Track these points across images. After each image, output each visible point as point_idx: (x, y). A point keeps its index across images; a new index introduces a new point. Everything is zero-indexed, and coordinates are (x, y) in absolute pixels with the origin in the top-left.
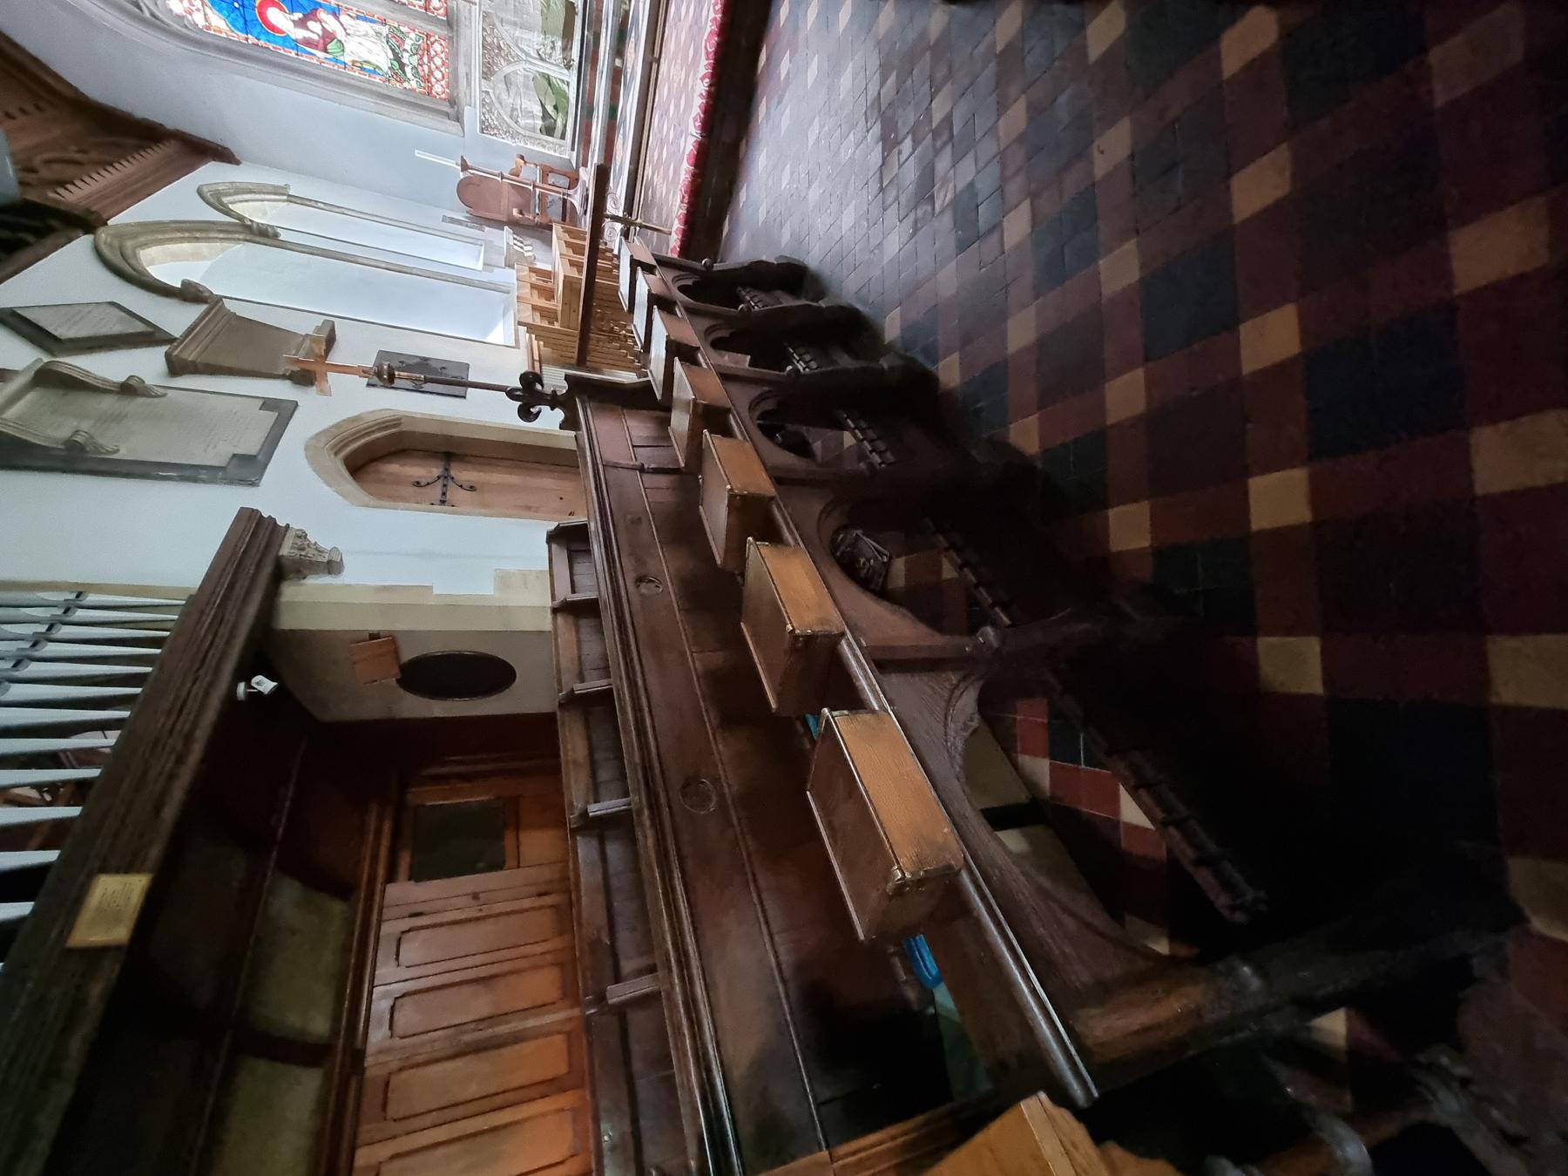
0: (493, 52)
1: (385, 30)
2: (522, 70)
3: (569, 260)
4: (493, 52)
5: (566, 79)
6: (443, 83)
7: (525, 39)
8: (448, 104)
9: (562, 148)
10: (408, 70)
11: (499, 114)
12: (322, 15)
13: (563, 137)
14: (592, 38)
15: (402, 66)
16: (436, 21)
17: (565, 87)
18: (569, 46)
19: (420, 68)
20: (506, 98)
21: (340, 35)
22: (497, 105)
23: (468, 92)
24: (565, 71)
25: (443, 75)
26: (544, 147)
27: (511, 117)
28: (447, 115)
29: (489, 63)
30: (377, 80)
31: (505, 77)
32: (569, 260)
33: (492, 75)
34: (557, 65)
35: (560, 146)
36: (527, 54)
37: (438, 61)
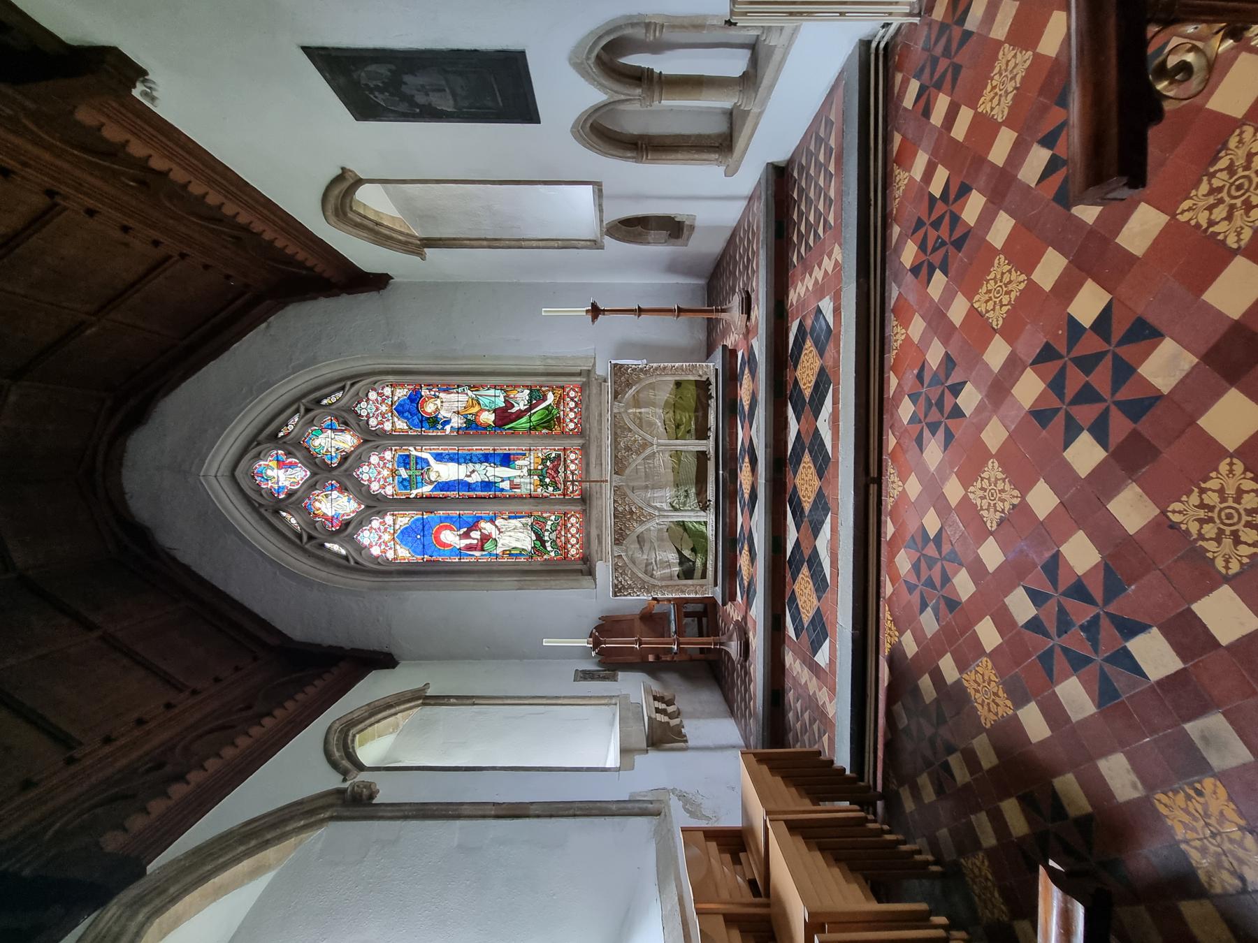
0: (624, 519)
1: (530, 521)
2: (656, 526)
3: (786, 821)
4: (624, 519)
6: (577, 546)
8: (581, 562)
10: (548, 544)
11: (633, 573)
12: (483, 524)
13: (704, 576)
15: (543, 543)
16: (573, 501)
18: (704, 489)
19: (558, 540)
21: (495, 533)
22: (631, 565)
24: (703, 513)
25: (577, 539)
26: (683, 592)
27: (646, 572)
28: (581, 572)
29: (621, 529)
30: (522, 560)
31: (638, 537)
32: (786, 821)
34: (692, 510)
35: (702, 586)
36: (660, 510)
37: (573, 530)
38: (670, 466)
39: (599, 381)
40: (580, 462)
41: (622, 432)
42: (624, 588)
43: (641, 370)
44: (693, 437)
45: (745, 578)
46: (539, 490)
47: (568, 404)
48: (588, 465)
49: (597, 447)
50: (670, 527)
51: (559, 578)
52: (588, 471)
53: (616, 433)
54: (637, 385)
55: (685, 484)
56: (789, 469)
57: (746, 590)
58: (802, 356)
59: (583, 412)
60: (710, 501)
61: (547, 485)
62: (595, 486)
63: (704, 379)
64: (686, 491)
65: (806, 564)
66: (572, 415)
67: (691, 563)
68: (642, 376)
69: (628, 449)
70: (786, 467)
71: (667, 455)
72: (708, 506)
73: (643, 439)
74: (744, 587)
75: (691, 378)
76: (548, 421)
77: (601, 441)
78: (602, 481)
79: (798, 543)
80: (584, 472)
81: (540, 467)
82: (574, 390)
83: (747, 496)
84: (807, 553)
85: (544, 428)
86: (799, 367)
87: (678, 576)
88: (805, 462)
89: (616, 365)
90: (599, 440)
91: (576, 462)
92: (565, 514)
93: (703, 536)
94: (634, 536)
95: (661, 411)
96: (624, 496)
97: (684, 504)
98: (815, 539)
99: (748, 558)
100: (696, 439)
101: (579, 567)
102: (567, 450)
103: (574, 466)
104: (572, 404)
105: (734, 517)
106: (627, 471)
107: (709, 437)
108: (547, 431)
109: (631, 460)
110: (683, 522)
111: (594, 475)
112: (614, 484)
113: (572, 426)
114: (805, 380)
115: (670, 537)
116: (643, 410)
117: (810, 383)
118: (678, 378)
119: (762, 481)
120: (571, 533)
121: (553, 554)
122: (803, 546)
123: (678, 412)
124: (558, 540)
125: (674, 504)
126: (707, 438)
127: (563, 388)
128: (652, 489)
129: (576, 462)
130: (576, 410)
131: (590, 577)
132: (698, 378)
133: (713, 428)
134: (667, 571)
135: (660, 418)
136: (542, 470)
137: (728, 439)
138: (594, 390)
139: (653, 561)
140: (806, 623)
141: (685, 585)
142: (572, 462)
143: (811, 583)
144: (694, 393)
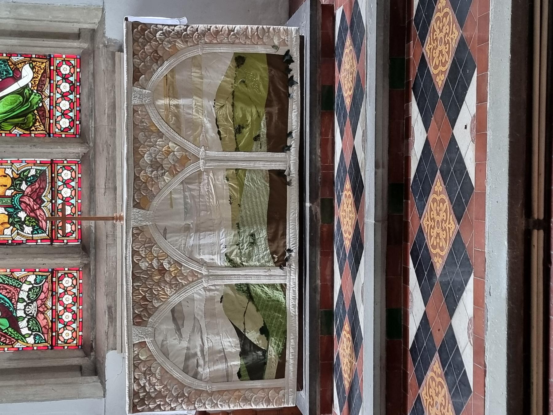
2: (202, 292)
5: (278, 281)
6: (74, 326)
7: (204, 245)
8: (80, 353)
9: (282, 392)
10: (23, 324)
11: (164, 371)
13: (280, 373)
14: (319, 210)
16: (67, 251)
17: (279, 295)
18: (280, 233)
19: (41, 316)
20: (176, 342)
22: (160, 359)
23: (111, 329)
24: (278, 271)
26: (246, 400)
27: (186, 370)
28: (80, 369)
29: (144, 298)
31: (173, 311)
33: (150, 315)
34: (262, 266)
35: (277, 390)
36: (210, 266)
37: (67, 299)
38: (226, 193)
39: (111, 49)
40: (79, 184)
41: (148, 137)
42: (150, 397)
43: (179, 35)
44: (265, 147)
45: (346, 376)
46: (8, 232)
47: (57, 86)
48: (92, 189)
49: (108, 160)
50: (227, 295)
51: (43, 381)
52: (92, 200)
53: (136, 140)
54: (172, 60)
55: (251, 225)
56: (412, 201)
57: (347, 395)
58: (433, 22)
59: (84, 100)
60: (290, 251)
61: (22, 223)
62: (105, 227)
63: (282, 52)
64: (252, 235)
65: (437, 354)
66: (65, 105)
67: (260, 353)
68: (180, 44)
69: (156, 165)
70: (407, 198)
71: (221, 176)
72: (287, 260)
73: (183, 149)
74: (344, 392)
75: (262, 50)
76: (24, 114)
77: (114, 150)
78: (113, 218)
79: (425, 321)
80: (86, 203)
81: (9, 193)
82: (68, 63)
83: (348, 244)
84: (438, 338)
85: (16, 125)
86: (428, 38)
87: (239, 375)
88: (436, 193)
89: (135, 24)
90: (112, 148)
91: (73, 184)
92: (53, 272)
93: (281, 309)
94: (166, 311)
95: (212, 103)
96: (150, 243)
97: (249, 256)
98: (451, 315)
99: (350, 344)
100: (269, 151)
101: (76, 361)
102: (57, 163)
103: (69, 191)
104: (65, 87)
105: (328, 278)
106: (155, 203)
107: (289, 148)
108: (21, 131)
109: (161, 184)
110: (247, 285)
111: (103, 209)
112: (133, 223)
113: (65, 123)
114: (436, 61)
115: (226, 309)
116: (181, 102)
117: (444, 65)
118: (239, 50)
119: (370, 220)
120: (62, 304)
121: (31, 340)
122: (433, 326)
123: (239, 105)
124: (41, 316)
125: (232, 257)
126: (285, 148)
127: (50, 59)
128: (198, 231)
129: (73, 184)
130: (71, 97)
131: (95, 378)
132: (272, 51)
133: (296, 134)
134: (221, 366)
135: (209, 114)
136: (12, 197)
137: (319, 151)
138: (103, 64)
139: (198, 350)
140: (436, 365)
141: (250, 390)
142: (66, 183)
143: (445, 386)
144: (266, 75)
